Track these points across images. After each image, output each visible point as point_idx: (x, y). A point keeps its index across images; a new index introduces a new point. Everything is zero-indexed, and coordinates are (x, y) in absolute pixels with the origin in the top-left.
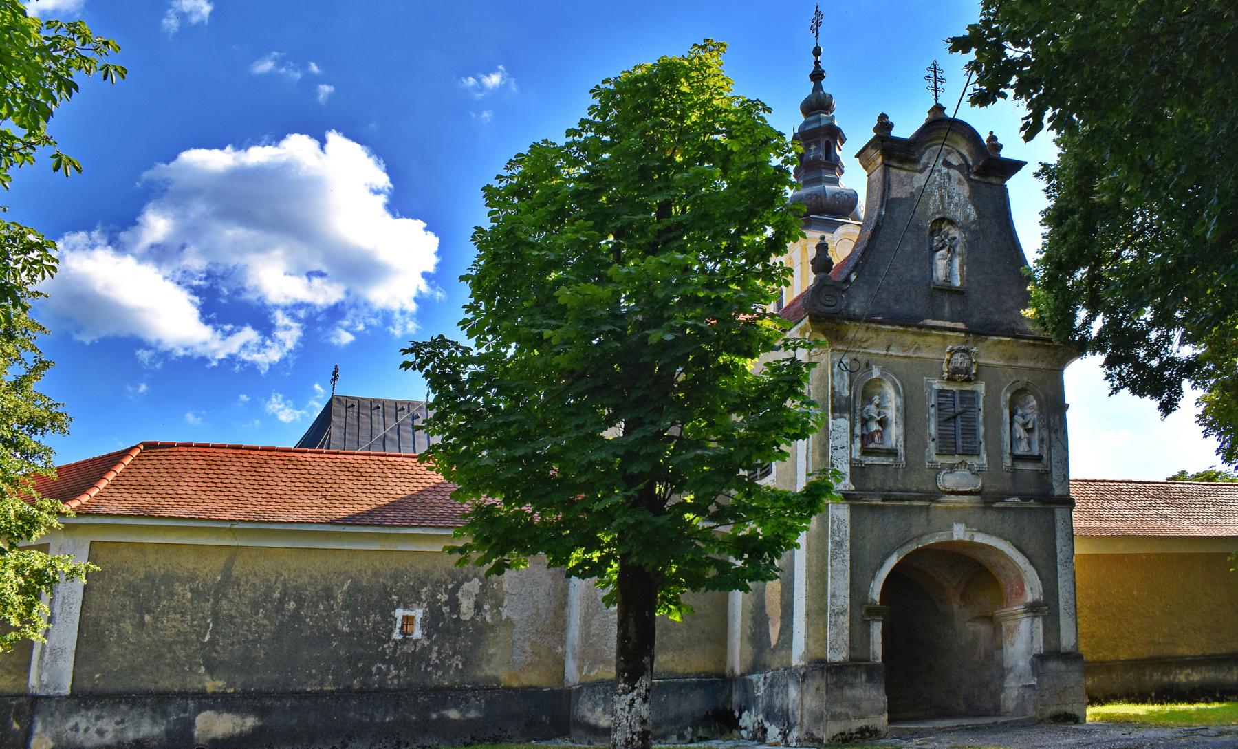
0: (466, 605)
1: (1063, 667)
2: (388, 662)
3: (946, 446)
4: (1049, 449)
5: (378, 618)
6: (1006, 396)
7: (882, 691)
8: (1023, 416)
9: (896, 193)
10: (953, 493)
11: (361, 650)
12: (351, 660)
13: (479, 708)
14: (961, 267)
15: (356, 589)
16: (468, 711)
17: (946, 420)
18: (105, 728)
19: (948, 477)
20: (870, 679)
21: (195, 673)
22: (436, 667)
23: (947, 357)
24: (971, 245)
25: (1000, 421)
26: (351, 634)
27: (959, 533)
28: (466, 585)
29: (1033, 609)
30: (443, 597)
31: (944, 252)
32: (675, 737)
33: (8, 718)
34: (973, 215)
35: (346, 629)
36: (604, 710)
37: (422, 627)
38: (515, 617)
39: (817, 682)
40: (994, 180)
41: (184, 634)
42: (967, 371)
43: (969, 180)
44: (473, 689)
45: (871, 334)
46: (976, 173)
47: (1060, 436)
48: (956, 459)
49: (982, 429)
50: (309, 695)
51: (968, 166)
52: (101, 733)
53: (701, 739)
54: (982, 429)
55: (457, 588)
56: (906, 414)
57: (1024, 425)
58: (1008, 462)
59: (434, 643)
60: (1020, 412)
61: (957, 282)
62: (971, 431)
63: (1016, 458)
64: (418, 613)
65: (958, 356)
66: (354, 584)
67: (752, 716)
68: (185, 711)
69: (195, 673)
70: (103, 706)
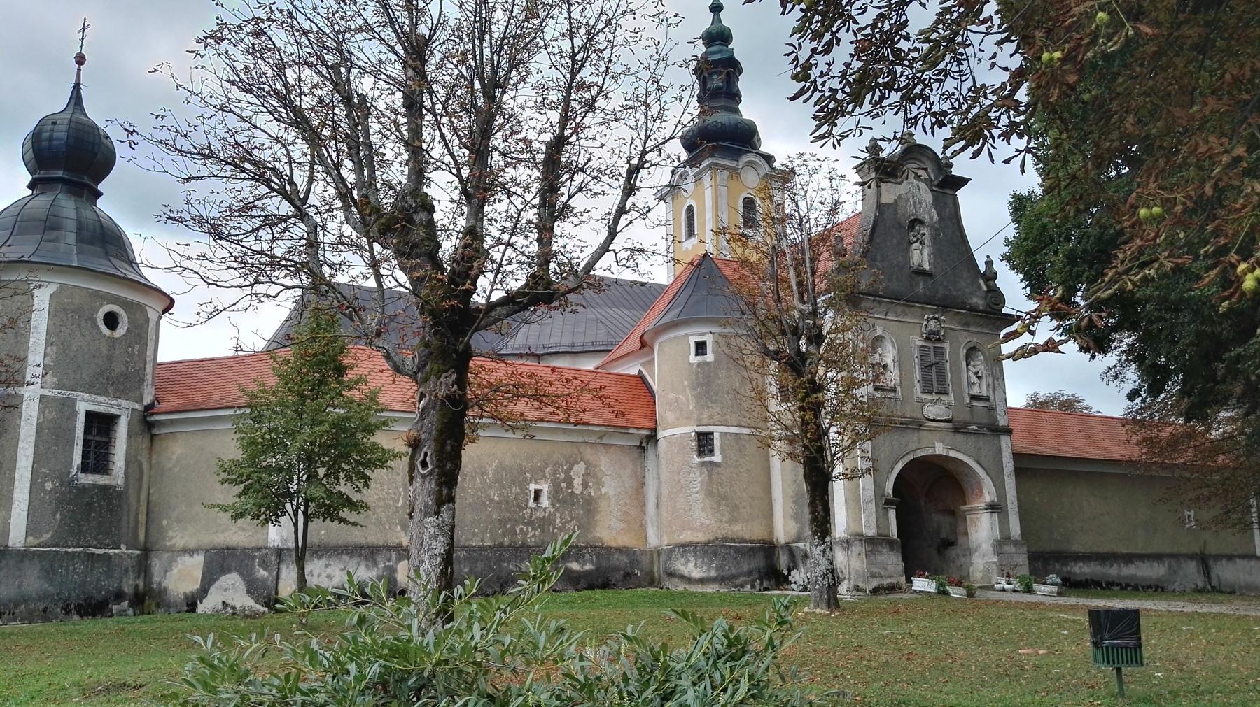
0: (577, 482)
1: (1013, 550)
2: (528, 524)
3: (927, 389)
4: (994, 392)
5: (518, 490)
6: (963, 352)
7: (900, 558)
8: (974, 366)
9: (883, 200)
10: (934, 420)
11: (508, 515)
12: (503, 522)
13: (591, 562)
14: (929, 255)
15: (501, 467)
16: (585, 564)
17: (926, 367)
18: (333, 574)
19: (930, 408)
20: (892, 549)
21: (393, 531)
22: (559, 528)
23: (925, 323)
24: (935, 239)
25: (960, 368)
26: (500, 503)
27: (939, 449)
28: (576, 467)
29: (993, 508)
30: (562, 476)
31: (918, 244)
32: (749, 586)
33: (253, 565)
34: (936, 218)
35: (497, 499)
36: (696, 564)
37: (549, 498)
38: (611, 493)
39: (857, 548)
40: (948, 191)
41: (384, 500)
42: (938, 333)
43: (932, 190)
44: (586, 547)
45: (876, 304)
46: (936, 186)
47: (1000, 382)
48: (935, 397)
49: (949, 375)
50: (474, 549)
51: (931, 181)
52: (329, 577)
53: (766, 589)
54: (949, 375)
55: (570, 468)
56: (900, 361)
57: (976, 373)
58: (967, 400)
59: (558, 510)
60: (972, 363)
61: (927, 267)
62: (941, 376)
63: (973, 398)
64: (545, 487)
65: (932, 322)
66: (500, 463)
67: (802, 574)
68: (389, 561)
69: (393, 531)
70: (330, 557)
